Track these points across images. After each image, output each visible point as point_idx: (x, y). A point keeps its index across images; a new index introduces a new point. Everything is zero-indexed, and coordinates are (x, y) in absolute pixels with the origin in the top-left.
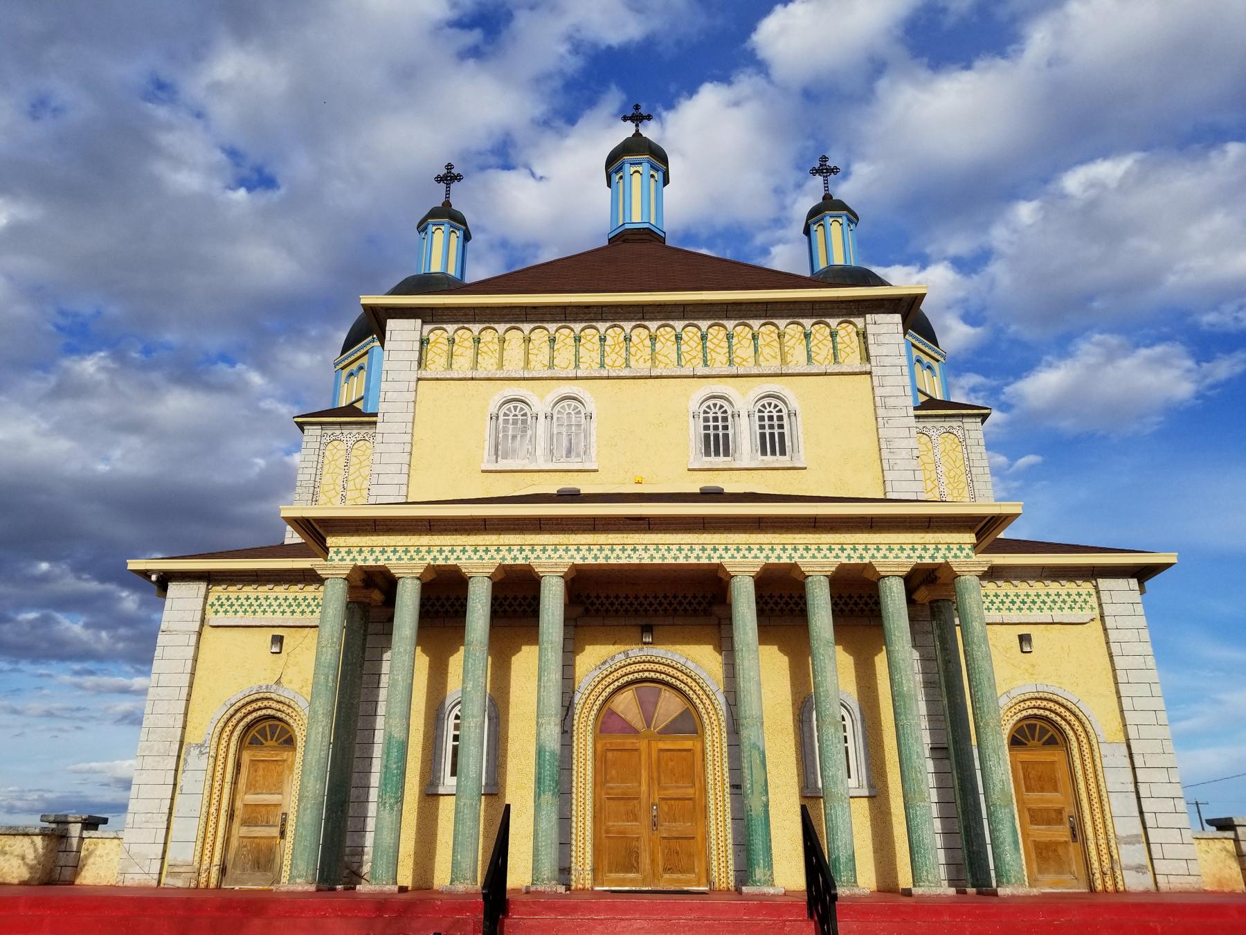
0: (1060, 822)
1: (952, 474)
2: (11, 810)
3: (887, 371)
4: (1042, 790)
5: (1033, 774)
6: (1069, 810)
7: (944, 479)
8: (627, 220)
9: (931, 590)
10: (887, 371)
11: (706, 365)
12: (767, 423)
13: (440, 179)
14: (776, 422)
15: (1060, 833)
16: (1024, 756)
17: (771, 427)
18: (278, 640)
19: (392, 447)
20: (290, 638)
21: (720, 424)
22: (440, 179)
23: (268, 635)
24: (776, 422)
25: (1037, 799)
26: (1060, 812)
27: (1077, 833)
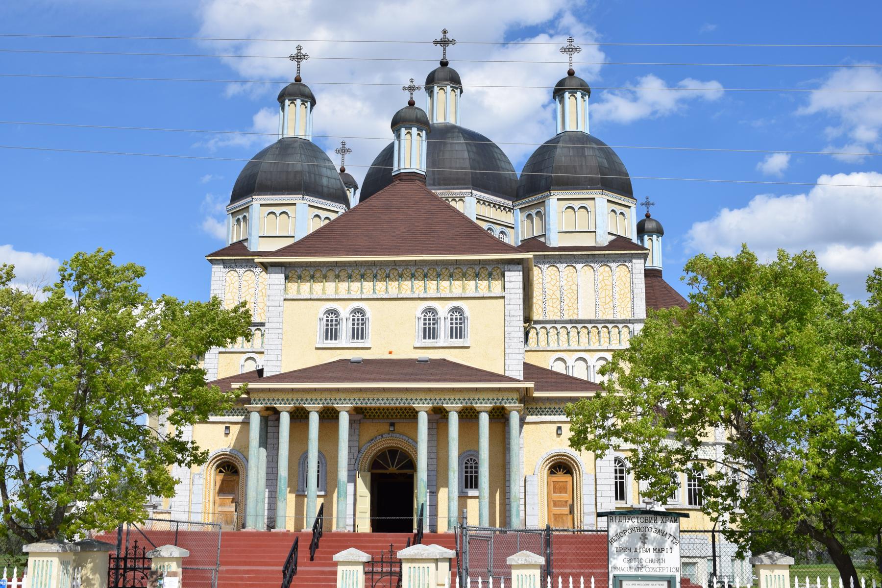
0: (566, 506)
1: (623, 292)
2: (794, 586)
3: (512, 296)
4: (560, 492)
5: (558, 486)
6: (570, 502)
7: (617, 296)
8: (402, 167)
9: (499, 417)
10: (512, 296)
11: (425, 292)
12: (454, 321)
13: (292, 58)
14: (458, 321)
15: (566, 510)
16: (554, 478)
17: (456, 324)
18: (227, 428)
19: (273, 336)
20: (232, 427)
21: (432, 322)
22: (292, 58)
23: (224, 426)
24: (458, 321)
25: (557, 496)
26: (566, 502)
27: (572, 512)
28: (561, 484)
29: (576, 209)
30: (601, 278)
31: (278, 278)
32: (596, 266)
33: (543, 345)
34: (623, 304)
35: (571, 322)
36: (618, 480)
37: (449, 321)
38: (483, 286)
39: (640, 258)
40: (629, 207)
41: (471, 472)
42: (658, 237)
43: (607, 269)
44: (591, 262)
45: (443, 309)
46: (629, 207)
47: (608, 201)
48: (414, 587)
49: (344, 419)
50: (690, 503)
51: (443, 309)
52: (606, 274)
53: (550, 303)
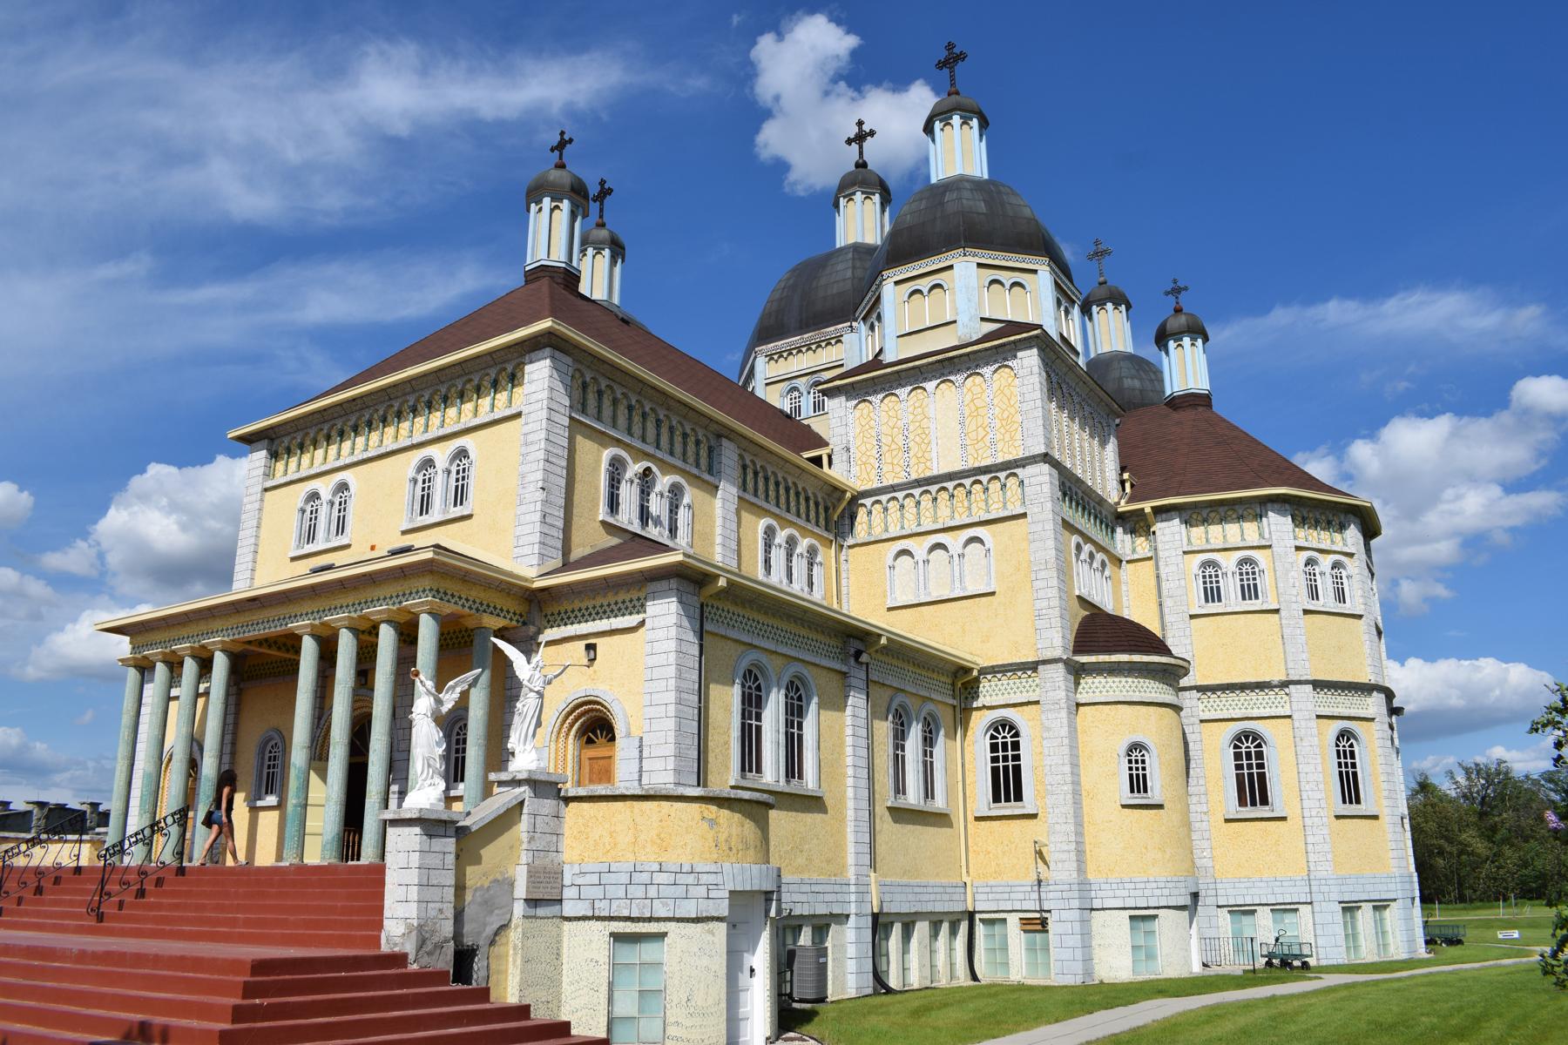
28: (601, 762)
29: (925, 291)
30: (968, 398)
31: (260, 457)
32: (958, 378)
33: (878, 533)
34: (1007, 437)
35: (918, 483)
36: (1010, 763)
37: (1238, 577)
38: (486, 407)
39: (1031, 347)
40: (1035, 272)
41: (1005, 759)
42: (1194, 339)
43: (978, 379)
44: (950, 373)
45: (1229, 562)
46: (1035, 272)
47: (980, 265)
48: (9, 990)
49: (220, 663)
50: (1242, 802)
51: (1229, 562)
52: (977, 390)
53: (887, 458)
